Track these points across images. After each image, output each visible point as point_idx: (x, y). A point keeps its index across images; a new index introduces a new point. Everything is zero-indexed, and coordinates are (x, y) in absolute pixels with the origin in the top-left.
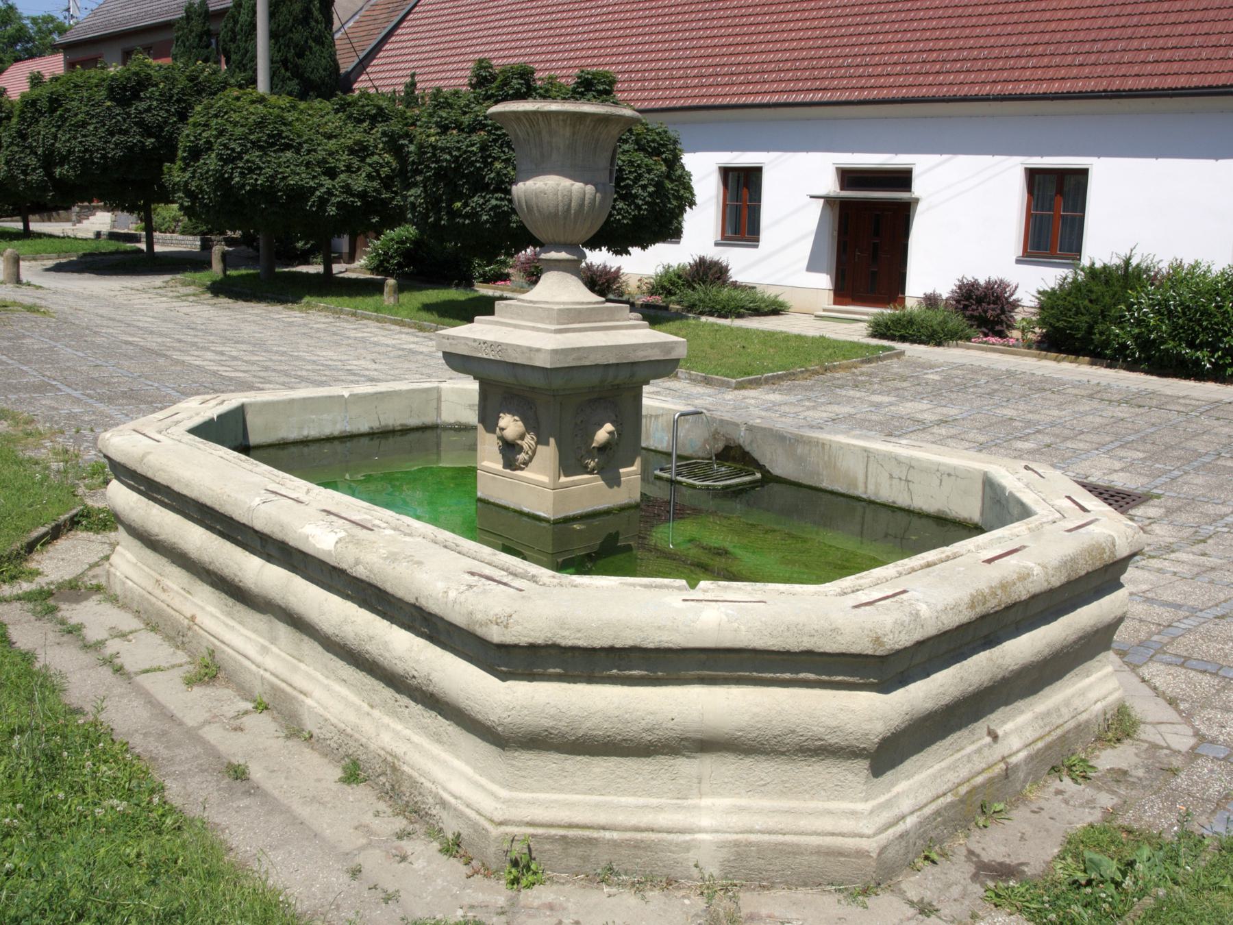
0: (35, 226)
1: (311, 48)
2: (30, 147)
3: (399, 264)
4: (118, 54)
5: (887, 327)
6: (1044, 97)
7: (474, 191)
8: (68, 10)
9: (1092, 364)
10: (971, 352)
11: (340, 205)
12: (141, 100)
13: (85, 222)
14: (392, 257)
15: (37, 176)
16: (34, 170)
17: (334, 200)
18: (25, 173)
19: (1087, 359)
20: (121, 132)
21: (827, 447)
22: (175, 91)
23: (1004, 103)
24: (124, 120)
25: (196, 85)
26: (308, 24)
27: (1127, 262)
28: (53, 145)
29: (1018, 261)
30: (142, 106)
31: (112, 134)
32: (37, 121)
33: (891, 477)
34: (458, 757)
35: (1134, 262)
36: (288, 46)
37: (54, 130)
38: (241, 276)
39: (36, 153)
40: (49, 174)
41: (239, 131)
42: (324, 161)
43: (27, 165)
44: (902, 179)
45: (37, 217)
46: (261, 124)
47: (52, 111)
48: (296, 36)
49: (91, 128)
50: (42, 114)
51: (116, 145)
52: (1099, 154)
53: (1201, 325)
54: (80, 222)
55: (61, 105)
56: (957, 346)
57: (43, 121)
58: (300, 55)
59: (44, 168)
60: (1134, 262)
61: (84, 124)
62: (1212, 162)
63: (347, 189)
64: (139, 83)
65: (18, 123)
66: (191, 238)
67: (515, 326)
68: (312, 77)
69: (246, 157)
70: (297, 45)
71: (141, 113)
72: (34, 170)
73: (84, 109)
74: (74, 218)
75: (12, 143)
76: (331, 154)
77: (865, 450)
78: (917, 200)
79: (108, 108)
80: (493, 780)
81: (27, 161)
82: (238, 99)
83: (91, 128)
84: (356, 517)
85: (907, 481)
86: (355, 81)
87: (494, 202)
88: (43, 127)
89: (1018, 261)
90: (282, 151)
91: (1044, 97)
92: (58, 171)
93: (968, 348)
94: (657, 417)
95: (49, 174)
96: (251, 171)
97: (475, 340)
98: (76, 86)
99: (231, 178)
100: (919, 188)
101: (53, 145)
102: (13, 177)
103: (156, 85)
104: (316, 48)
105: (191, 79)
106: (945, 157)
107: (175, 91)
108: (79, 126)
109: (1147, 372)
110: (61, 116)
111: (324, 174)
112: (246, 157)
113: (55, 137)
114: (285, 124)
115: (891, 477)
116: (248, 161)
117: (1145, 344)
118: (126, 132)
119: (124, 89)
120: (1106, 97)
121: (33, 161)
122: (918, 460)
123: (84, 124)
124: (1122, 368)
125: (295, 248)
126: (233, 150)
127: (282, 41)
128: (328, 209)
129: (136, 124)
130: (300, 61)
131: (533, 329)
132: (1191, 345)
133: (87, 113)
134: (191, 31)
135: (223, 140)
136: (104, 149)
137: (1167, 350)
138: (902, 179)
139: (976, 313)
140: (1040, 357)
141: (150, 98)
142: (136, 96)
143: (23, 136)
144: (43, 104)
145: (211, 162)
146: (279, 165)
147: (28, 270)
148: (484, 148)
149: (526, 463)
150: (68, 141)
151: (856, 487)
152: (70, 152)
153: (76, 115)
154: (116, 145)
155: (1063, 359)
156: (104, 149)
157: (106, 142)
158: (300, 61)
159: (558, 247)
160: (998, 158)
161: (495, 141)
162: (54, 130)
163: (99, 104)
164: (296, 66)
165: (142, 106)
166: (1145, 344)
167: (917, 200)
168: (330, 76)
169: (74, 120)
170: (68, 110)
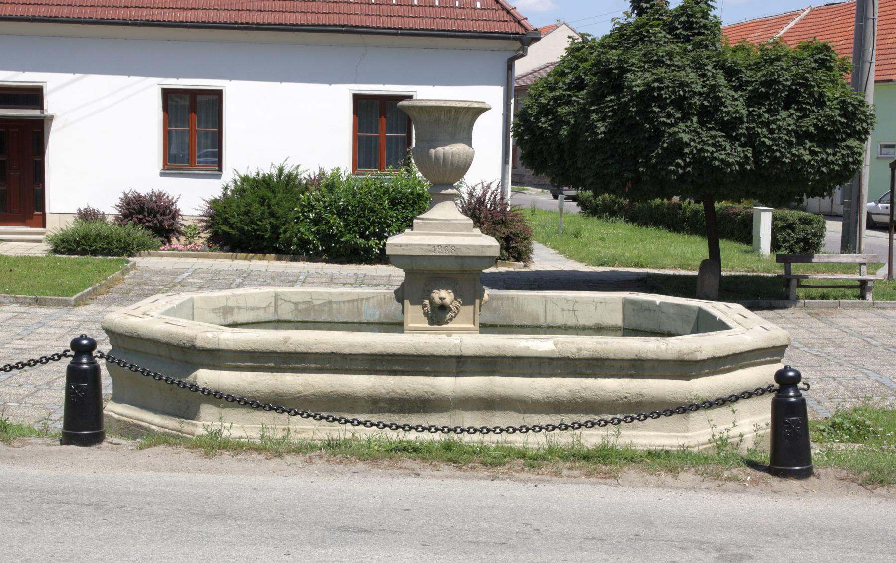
5: (78, 244)
6: (136, 24)
9: (279, 259)
10: (165, 259)
19: (273, 255)
21: (515, 300)
23: (85, 26)
27: (281, 170)
29: (162, 174)
33: (563, 310)
34: (649, 430)
35: (286, 172)
44: (33, 96)
52: (231, 77)
53: (369, 220)
56: (150, 255)
60: (286, 172)
62: (326, 86)
67: (446, 235)
77: (544, 297)
78: (51, 118)
80: (679, 432)
85: (574, 310)
89: (162, 174)
91: (136, 24)
93: (161, 256)
94: (368, 299)
97: (429, 245)
100: (51, 105)
106: (77, 75)
109: (327, 262)
115: (563, 310)
117: (326, 238)
120: (186, 27)
122: (580, 297)
124: (303, 260)
131: (463, 235)
132: (362, 236)
137: (347, 242)
138: (33, 96)
139: (151, 224)
140: (233, 259)
149: (451, 319)
151: (538, 319)
155: (252, 258)
160: (134, 79)
166: (326, 238)
167: (51, 118)
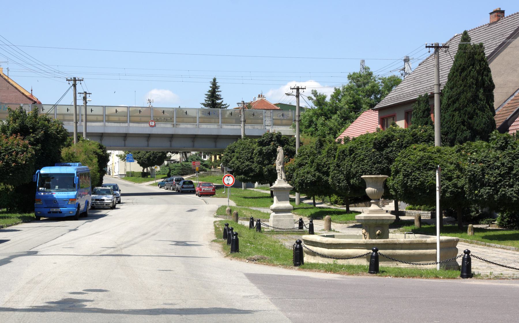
0: (351, 209)
1: (477, 114)
2: (341, 171)
3: (508, 221)
4: (403, 115)
7: (481, 187)
8: (404, 69)
11: (451, 192)
12: (388, 147)
13: (386, 206)
14: (505, 218)
15: (344, 184)
16: (343, 181)
17: (449, 190)
18: (339, 183)
20: (378, 163)
22: (404, 142)
24: (380, 157)
25: (415, 138)
26: (476, 102)
28: (350, 169)
30: (389, 150)
31: (375, 164)
32: (344, 159)
36: (465, 114)
37: (351, 163)
38: (426, 228)
39: (343, 174)
40: (349, 182)
41: (412, 163)
42: (446, 174)
43: (340, 179)
45: (353, 205)
46: (420, 160)
47: (351, 154)
48: (469, 109)
49: (366, 161)
50: (347, 156)
51: (376, 168)
54: (384, 206)
55: (354, 152)
57: (347, 159)
58: (471, 118)
59: (347, 180)
61: (363, 160)
63: (455, 186)
64: (387, 140)
65: (337, 160)
66: (426, 212)
68: (477, 128)
69: (413, 174)
70: (469, 113)
71: (387, 153)
72: (343, 181)
73: (364, 153)
74: (381, 204)
75: (334, 170)
76: (450, 171)
79: (373, 152)
81: (340, 177)
82: (415, 149)
83: (366, 161)
84: (325, 235)
86: (510, 126)
87: (487, 191)
88: (347, 162)
90: (429, 170)
92: (352, 181)
95: (349, 182)
96: (415, 179)
98: (361, 143)
99: (407, 182)
101: (350, 169)
102: (334, 185)
103: (396, 140)
104: (480, 113)
105: (413, 135)
107: (404, 142)
108: (361, 161)
110: (354, 157)
111: (446, 179)
112: (413, 174)
113: (351, 166)
114: (432, 159)
116: (414, 176)
118: (380, 163)
119: (380, 143)
121: (342, 177)
123: (363, 160)
125: (471, 216)
126: (408, 171)
127: (462, 112)
128: (446, 194)
129: (385, 158)
130: (470, 121)
133: (365, 155)
134: (420, 109)
135: (405, 167)
136: (371, 171)
141: (392, 146)
142: (386, 146)
143: (338, 166)
144: (347, 152)
145: (401, 177)
146: (427, 177)
147: (333, 226)
148: (483, 170)
150: (356, 168)
152: (357, 172)
153: (360, 156)
154: (376, 168)
156: (371, 171)
157: (372, 168)
158: (470, 121)
159: (373, 200)
161: (488, 167)
162: (351, 163)
163: (370, 151)
164: (469, 124)
165: (389, 150)
168: (488, 127)
169: (359, 158)
170: (356, 154)
